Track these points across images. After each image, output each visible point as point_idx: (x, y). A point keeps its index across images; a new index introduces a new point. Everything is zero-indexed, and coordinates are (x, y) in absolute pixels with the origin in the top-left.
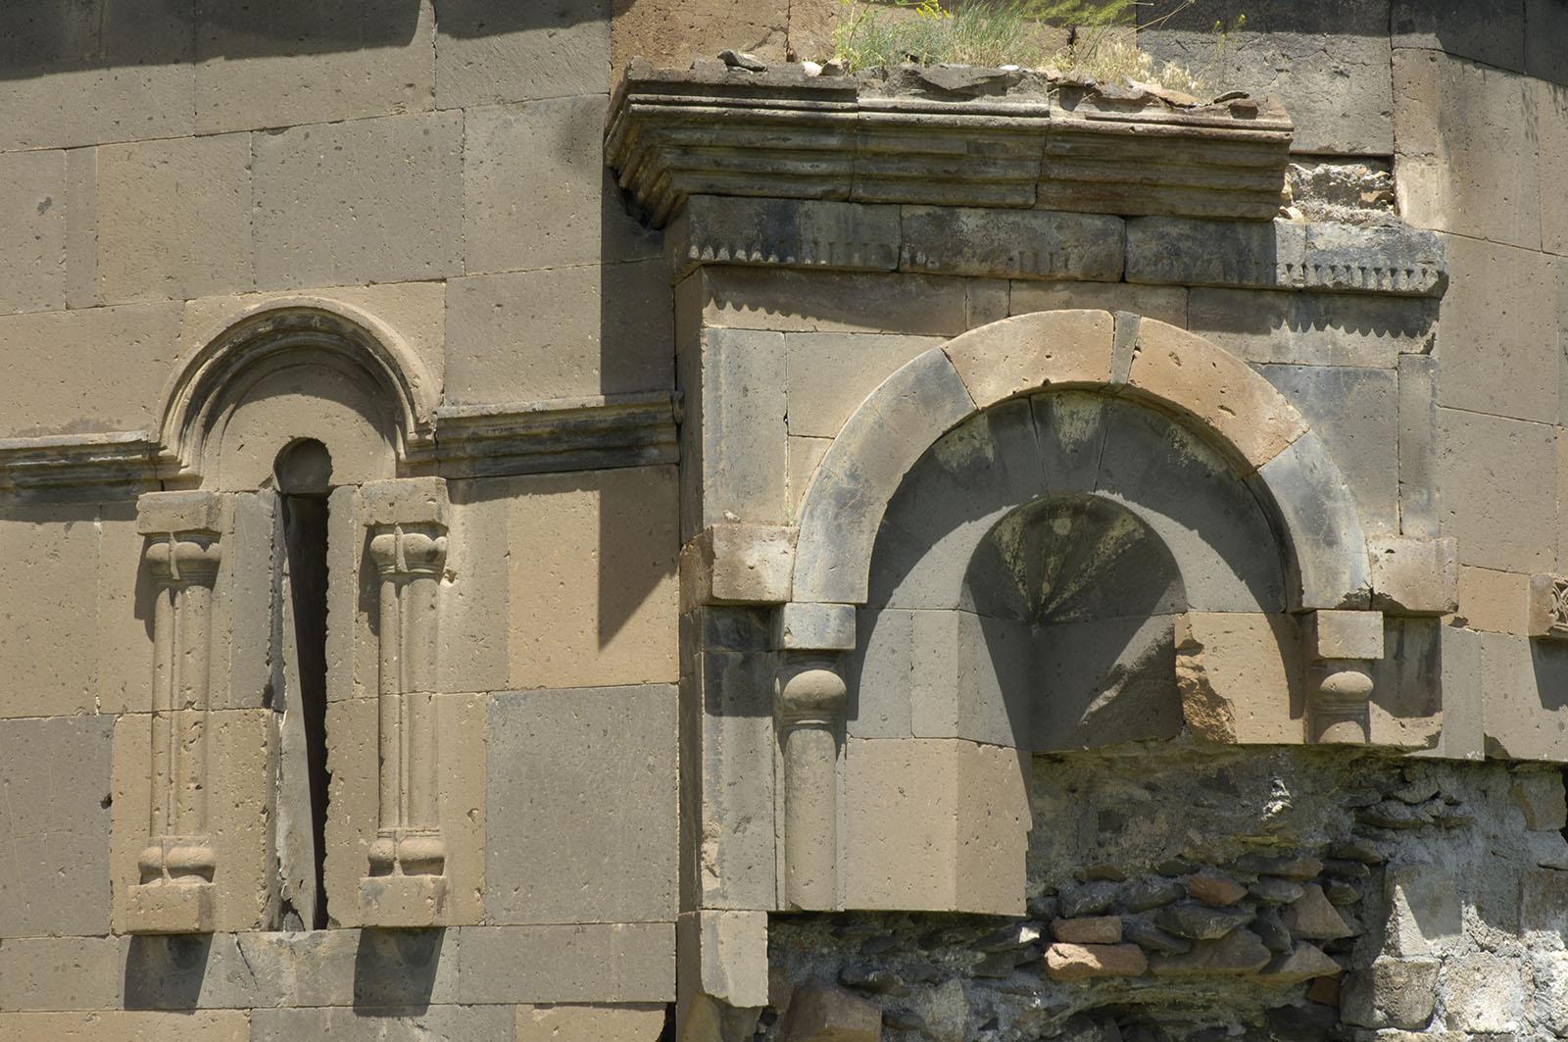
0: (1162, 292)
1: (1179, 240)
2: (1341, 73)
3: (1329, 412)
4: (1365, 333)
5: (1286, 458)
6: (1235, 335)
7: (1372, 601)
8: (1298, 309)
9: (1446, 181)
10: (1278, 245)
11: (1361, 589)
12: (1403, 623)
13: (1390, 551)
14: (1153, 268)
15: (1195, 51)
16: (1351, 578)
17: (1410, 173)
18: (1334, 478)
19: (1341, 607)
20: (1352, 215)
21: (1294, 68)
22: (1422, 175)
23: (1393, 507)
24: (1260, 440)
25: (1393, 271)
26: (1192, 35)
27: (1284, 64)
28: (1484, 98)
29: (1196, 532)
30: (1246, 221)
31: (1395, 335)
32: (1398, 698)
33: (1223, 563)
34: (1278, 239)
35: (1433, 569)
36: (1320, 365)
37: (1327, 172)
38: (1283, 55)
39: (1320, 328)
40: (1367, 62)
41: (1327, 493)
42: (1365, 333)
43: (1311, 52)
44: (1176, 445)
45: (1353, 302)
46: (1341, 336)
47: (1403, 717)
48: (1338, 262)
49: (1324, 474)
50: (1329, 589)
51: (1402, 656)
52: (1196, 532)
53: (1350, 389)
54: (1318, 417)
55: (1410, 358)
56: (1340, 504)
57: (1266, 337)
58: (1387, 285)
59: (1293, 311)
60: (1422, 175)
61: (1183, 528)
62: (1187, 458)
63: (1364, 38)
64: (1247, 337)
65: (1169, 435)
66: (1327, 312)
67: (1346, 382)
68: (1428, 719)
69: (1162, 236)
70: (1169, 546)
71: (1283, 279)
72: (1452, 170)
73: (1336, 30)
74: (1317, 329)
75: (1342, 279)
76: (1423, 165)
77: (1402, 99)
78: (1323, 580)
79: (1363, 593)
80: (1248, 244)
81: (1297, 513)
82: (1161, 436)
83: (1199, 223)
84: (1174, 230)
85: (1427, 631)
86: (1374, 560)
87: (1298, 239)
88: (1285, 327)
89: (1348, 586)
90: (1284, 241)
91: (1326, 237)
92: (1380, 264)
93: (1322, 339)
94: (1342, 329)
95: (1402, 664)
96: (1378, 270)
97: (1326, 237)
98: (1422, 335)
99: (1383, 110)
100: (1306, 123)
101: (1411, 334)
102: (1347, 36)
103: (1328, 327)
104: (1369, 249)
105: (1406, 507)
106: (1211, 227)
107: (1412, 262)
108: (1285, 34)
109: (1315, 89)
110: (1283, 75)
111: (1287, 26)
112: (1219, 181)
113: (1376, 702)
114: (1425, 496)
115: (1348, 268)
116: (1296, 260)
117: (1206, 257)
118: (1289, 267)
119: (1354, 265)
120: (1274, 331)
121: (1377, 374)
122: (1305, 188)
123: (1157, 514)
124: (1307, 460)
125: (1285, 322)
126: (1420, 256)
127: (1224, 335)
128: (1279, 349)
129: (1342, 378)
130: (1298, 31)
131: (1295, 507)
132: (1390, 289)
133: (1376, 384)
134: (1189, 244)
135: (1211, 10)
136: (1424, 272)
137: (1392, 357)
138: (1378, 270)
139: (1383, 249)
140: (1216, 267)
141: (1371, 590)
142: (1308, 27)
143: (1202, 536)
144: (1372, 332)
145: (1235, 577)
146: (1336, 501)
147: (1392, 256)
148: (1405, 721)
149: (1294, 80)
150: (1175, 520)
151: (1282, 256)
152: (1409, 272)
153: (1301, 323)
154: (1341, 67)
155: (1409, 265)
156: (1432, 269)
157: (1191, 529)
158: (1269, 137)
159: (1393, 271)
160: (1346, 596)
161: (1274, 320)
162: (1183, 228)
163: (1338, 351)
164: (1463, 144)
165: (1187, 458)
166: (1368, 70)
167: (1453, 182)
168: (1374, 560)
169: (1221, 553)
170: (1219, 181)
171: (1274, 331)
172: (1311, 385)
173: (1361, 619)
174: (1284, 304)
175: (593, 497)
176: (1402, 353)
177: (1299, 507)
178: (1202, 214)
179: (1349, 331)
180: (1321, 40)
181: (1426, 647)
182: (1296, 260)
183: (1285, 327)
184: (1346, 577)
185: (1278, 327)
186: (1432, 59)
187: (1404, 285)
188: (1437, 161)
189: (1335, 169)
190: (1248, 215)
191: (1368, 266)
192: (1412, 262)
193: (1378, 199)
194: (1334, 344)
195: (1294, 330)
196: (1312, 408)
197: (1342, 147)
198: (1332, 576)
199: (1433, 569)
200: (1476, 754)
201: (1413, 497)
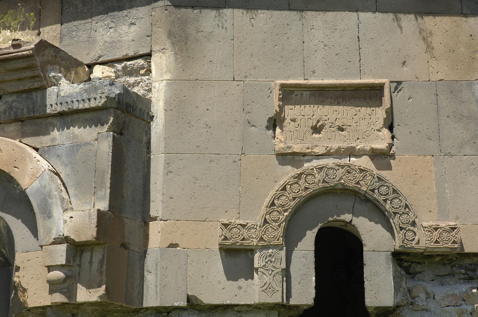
0: (13, 124)
1: (12, 103)
2: (133, 24)
3: (70, 162)
4: (85, 128)
5: (36, 184)
6: (37, 137)
7: (66, 240)
8: (60, 122)
9: (172, 58)
10: (47, 97)
11: (60, 235)
12: (93, 248)
13: (72, 217)
14: (4, 116)
15: (81, 28)
16: (56, 231)
17: (156, 58)
18: (52, 189)
19: (53, 243)
20: (136, 80)
21: (116, 26)
22: (160, 58)
23: (91, 199)
24: (27, 178)
25: (89, 100)
26: (80, 22)
27: (112, 25)
28: (198, 21)
29: (20, 220)
30: (37, 89)
31: (96, 126)
32: (89, 281)
33: (29, 232)
34: (47, 95)
35: (87, 222)
36: (67, 144)
37: (125, 65)
38: (112, 22)
39: (68, 128)
40: (142, 17)
41: (50, 196)
42: (85, 128)
43: (121, 18)
44: (15, 185)
45: (81, 115)
46: (76, 130)
47: (90, 289)
48: (69, 100)
49: (49, 188)
50: (48, 236)
51: (92, 262)
52: (20, 220)
53: (78, 152)
54: (66, 165)
55: (102, 135)
56: (54, 200)
57: (48, 136)
58: (87, 106)
59: (59, 123)
60: (160, 58)
61: (16, 219)
62: (19, 190)
63: (141, 8)
64: (42, 137)
65: (13, 182)
66: (71, 121)
67: (77, 149)
68: (99, 289)
69: (6, 102)
70: (10, 227)
71: (48, 111)
72: (176, 54)
73: (131, 7)
74: (67, 129)
75: (70, 107)
76: (161, 54)
77: (154, 28)
78: (46, 233)
79: (61, 237)
80: (37, 99)
81: (38, 206)
82: (10, 182)
83: (19, 94)
84: (10, 99)
85: (101, 250)
86: (65, 222)
87: (54, 93)
88: (56, 130)
89: (55, 234)
90: (49, 95)
91: (65, 91)
92: (84, 98)
93: (69, 133)
94: (77, 127)
95: (91, 266)
96: (83, 100)
97: (65, 91)
98: (107, 124)
99: (147, 35)
100: (118, 47)
101: (102, 125)
102: (135, 8)
103: (71, 128)
104: (80, 92)
105: (97, 198)
106: (24, 95)
107: (96, 94)
108: (113, 13)
109: (122, 32)
110: (112, 30)
111: (113, 10)
112: (16, 76)
113: (80, 284)
114: (104, 192)
115: (72, 102)
116: (53, 103)
117: (21, 108)
118: (51, 105)
119: (74, 100)
120: (52, 133)
121: (88, 143)
122: (120, 73)
123: (7, 215)
124: (43, 184)
125: (55, 128)
126: (100, 91)
127: (34, 138)
128: (53, 140)
129: (77, 146)
130: (117, 11)
131: (38, 204)
132: (88, 107)
133: (89, 147)
134: (16, 103)
135: (87, 10)
136: (101, 97)
137: (95, 135)
138: (83, 100)
139: (85, 91)
140: (25, 111)
141: (63, 235)
142: (121, 8)
143: (22, 222)
144: (88, 127)
145: (33, 237)
146: (52, 199)
147: (89, 94)
148: (90, 290)
149: (116, 31)
150: (13, 216)
151: (48, 102)
152: (95, 99)
153: (61, 128)
154: (133, 21)
155: (95, 96)
156: (103, 96)
157: (18, 219)
158: (23, 54)
159: (89, 100)
160: (54, 239)
161: (51, 128)
162: (14, 97)
163: (75, 136)
164: (182, 42)
165: (19, 190)
166: (143, 20)
167: (176, 59)
168: (65, 222)
169: (28, 228)
170: (16, 76)
171: (52, 133)
172: (64, 152)
173: (58, 248)
174: (55, 121)
175: (77, 300)
176: (99, 133)
177: (39, 204)
178: (16, 90)
179: (79, 128)
180: (125, 12)
181: (101, 257)
182: (53, 103)
183: (56, 130)
184: (54, 231)
185: (53, 131)
186: (166, 10)
187: (93, 104)
188: (166, 51)
189: (129, 63)
190: (31, 87)
191: (79, 99)
192: (96, 94)
193: (146, 71)
194: (73, 134)
195: (59, 131)
196: (63, 162)
197: (131, 54)
198: (49, 231)
199: (87, 222)
200: (183, 303)
201: (99, 193)
